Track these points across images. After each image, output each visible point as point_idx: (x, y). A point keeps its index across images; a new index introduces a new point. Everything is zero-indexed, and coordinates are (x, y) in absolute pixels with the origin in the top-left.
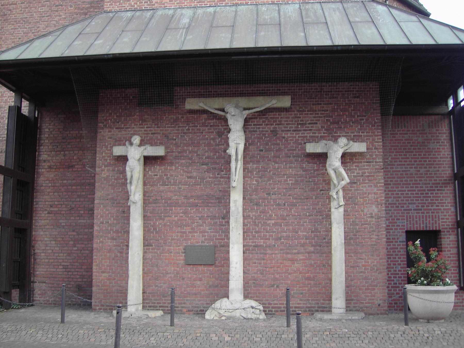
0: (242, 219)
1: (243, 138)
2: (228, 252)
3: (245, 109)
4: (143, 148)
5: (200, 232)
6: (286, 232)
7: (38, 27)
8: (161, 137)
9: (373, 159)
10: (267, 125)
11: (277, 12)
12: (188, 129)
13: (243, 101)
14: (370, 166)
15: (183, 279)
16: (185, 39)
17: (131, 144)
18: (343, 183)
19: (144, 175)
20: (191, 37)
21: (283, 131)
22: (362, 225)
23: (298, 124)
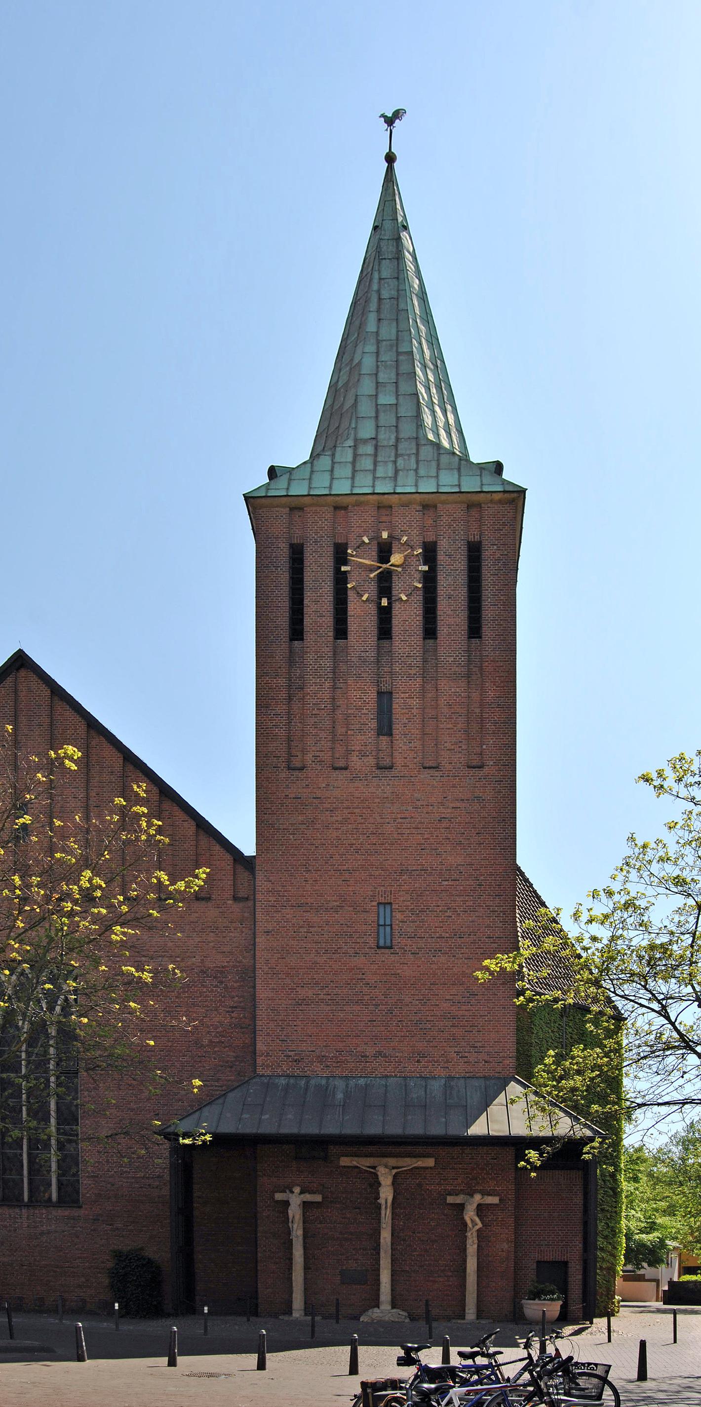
0: (390, 1251)
1: (392, 1191)
2: (379, 1275)
3: (394, 1168)
4: (302, 1196)
5: (354, 1260)
6: (428, 1261)
7: (181, 1076)
8: (317, 1185)
9: (507, 1208)
10: (413, 1179)
11: (423, 1089)
12: (342, 1181)
13: (392, 1161)
14: (503, 1213)
15: (339, 1294)
16: (343, 1119)
17: (292, 1192)
18: (477, 1227)
19: (303, 1216)
20: (348, 1117)
21: (427, 1184)
22: (494, 1257)
23: (441, 1180)
